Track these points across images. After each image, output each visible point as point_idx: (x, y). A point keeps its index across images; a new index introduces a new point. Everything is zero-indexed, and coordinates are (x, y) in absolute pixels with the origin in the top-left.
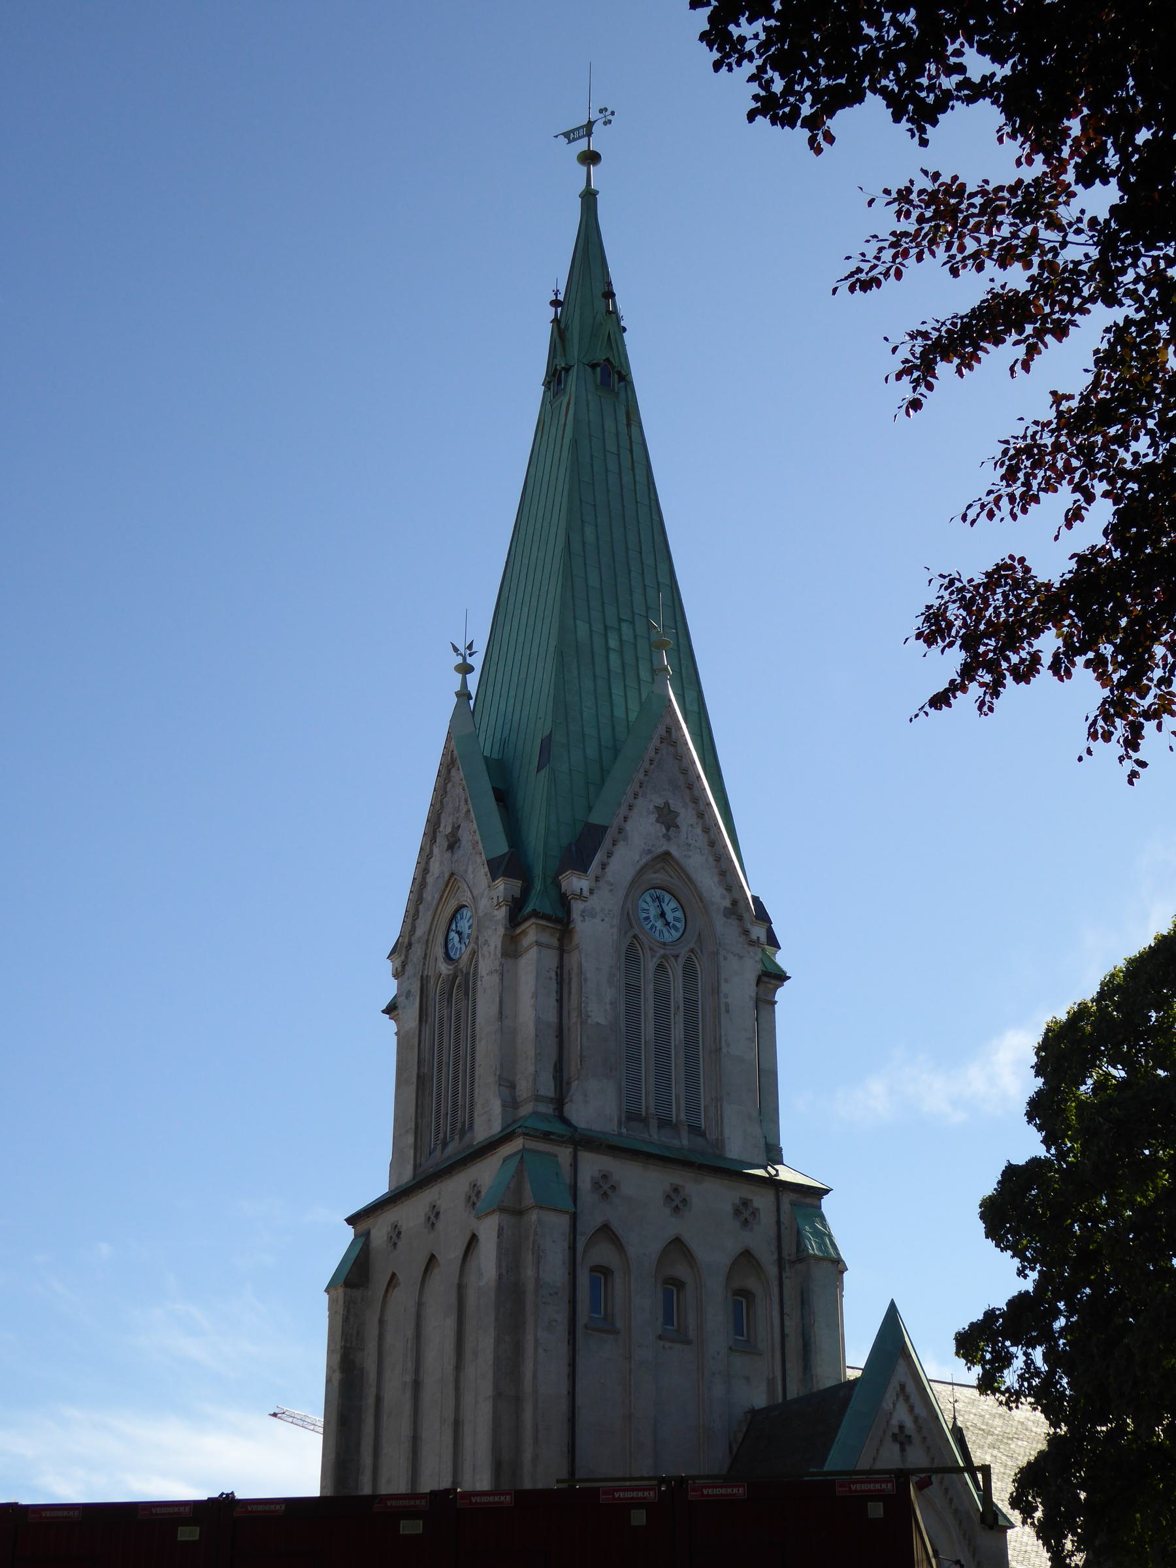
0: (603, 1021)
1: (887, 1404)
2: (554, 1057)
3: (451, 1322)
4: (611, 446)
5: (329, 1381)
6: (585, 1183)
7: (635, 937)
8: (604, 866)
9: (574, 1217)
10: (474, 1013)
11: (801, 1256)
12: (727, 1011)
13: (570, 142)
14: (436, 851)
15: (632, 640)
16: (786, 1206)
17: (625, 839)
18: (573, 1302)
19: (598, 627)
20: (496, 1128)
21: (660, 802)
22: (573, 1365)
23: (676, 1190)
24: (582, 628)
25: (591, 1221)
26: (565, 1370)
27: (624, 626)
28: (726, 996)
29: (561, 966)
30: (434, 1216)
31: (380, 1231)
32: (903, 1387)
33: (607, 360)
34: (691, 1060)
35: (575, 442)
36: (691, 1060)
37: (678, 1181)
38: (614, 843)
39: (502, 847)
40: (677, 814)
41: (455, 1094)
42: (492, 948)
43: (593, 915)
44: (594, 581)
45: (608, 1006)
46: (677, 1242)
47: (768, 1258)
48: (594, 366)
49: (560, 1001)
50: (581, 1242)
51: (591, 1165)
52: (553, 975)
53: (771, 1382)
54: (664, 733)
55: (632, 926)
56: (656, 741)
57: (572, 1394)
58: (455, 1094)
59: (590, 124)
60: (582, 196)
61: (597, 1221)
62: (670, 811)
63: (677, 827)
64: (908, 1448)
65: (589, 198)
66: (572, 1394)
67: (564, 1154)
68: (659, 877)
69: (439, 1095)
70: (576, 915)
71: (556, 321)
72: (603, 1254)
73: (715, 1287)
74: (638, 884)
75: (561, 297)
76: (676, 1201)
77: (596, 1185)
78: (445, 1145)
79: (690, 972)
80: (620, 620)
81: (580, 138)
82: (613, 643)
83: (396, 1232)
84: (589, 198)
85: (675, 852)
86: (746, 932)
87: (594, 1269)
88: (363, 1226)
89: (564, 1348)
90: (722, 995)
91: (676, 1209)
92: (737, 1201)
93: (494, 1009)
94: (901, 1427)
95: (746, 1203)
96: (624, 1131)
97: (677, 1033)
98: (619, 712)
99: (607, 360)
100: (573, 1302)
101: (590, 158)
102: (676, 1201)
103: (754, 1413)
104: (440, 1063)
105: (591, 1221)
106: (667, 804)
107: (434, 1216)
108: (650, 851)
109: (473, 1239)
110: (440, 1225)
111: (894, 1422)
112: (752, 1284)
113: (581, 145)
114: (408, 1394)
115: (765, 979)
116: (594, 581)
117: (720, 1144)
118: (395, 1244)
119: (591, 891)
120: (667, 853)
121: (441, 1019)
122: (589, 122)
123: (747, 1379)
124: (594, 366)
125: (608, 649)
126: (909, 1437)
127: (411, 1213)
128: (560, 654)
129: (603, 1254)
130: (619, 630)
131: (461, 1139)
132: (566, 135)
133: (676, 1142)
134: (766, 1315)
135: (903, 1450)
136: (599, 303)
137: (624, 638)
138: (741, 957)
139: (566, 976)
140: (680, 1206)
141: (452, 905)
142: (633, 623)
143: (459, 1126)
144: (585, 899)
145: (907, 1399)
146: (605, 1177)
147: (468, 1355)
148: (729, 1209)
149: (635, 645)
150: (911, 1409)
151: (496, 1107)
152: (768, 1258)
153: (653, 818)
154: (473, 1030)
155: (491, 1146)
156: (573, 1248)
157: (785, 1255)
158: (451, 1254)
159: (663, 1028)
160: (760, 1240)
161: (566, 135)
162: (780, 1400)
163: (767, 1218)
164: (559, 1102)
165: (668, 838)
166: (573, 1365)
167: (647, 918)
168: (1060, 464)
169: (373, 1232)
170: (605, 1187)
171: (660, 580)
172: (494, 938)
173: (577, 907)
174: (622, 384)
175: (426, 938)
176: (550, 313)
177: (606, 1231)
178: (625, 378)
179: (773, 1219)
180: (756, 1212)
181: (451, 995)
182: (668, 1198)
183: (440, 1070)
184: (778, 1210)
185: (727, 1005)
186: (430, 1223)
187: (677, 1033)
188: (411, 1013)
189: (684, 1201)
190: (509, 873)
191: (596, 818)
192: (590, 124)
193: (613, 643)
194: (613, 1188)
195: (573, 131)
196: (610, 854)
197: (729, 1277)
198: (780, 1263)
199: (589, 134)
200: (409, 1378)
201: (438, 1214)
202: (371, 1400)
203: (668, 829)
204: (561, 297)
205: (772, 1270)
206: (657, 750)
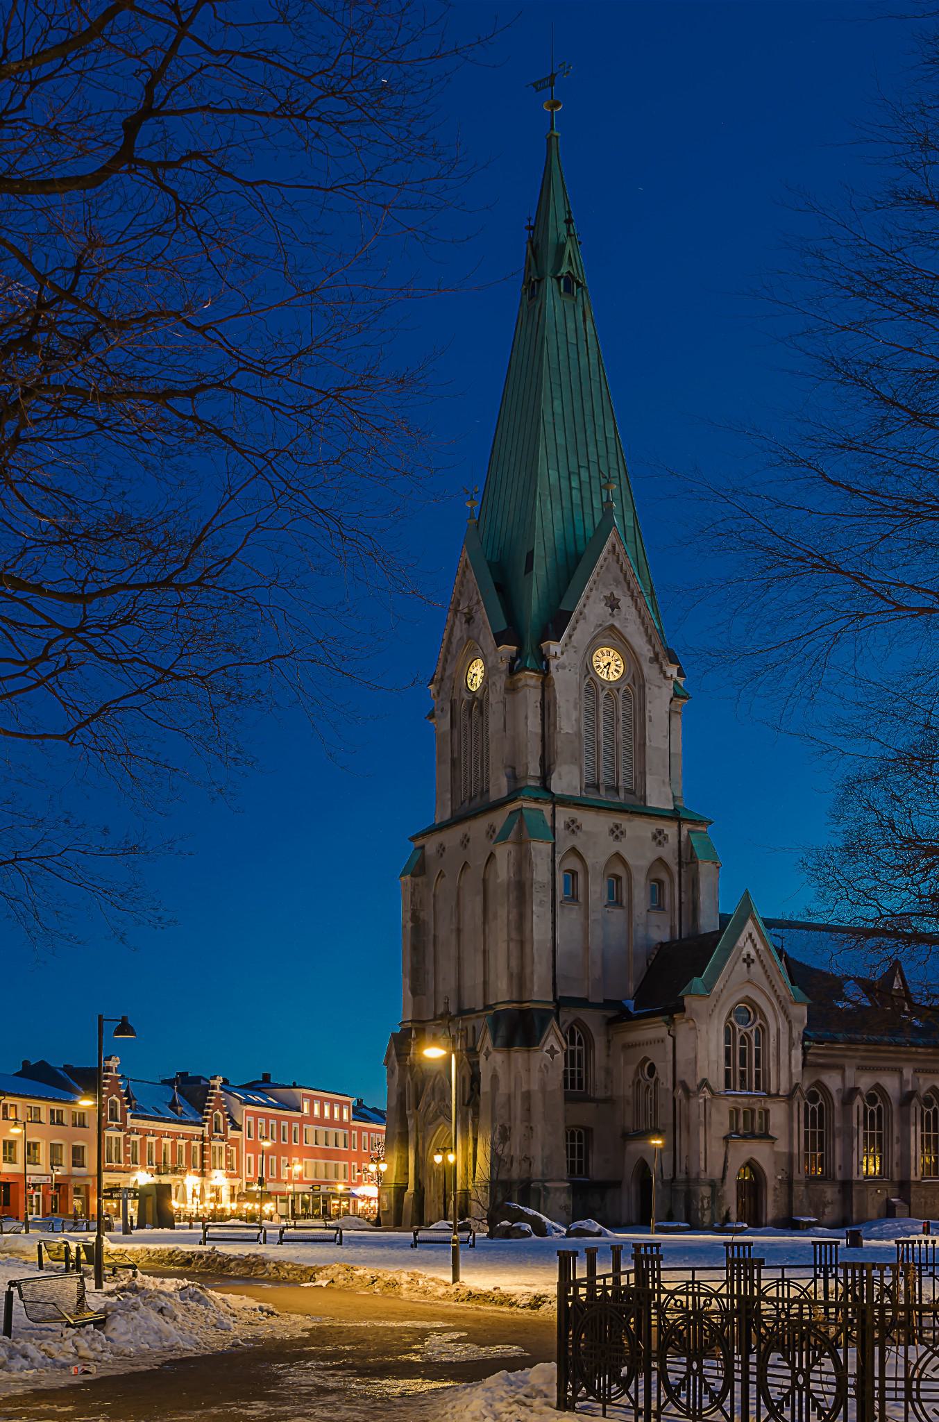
1: (740, 943)
2: (540, 752)
6: (560, 825)
7: (591, 679)
8: (570, 637)
10: (487, 725)
12: (650, 721)
13: (537, 91)
14: (457, 622)
18: (554, 890)
19: (564, 473)
20: (505, 793)
21: (608, 593)
22: (554, 923)
23: (617, 827)
26: (550, 925)
27: (582, 470)
30: (465, 841)
32: (750, 935)
33: (569, 272)
37: (618, 822)
38: (577, 622)
39: (503, 625)
40: (619, 600)
41: (476, 771)
43: (564, 668)
46: (618, 855)
50: (558, 860)
51: (563, 814)
53: (672, 928)
54: (611, 548)
55: (589, 673)
61: (569, 846)
62: (615, 599)
64: (752, 966)
67: (547, 809)
70: (552, 669)
76: (617, 833)
77: (568, 826)
78: (471, 799)
82: (575, 484)
83: (442, 849)
85: (617, 625)
86: (664, 673)
89: (549, 916)
94: (749, 955)
95: (660, 832)
96: (584, 794)
98: (580, 532)
99: (569, 272)
100: (554, 890)
103: (662, 944)
106: (612, 594)
108: (601, 625)
110: (470, 845)
111: (744, 952)
112: (663, 876)
116: (561, 440)
120: (613, 626)
121: (465, 726)
123: (658, 926)
125: (571, 488)
126: (753, 961)
131: (481, 797)
132: (534, 85)
133: (616, 800)
135: (749, 966)
137: (582, 479)
138: (660, 687)
142: (588, 468)
145: (753, 941)
146: (573, 822)
147: (490, 916)
150: (755, 946)
151: (504, 781)
153: (603, 604)
156: (553, 861)
166: (554, 923)
167: (599, 666)
168: (780, 1307)
170: (573, 826)
173: (553, 663)
180: (666, 837)
181: (471, 712)
182: (612, 832)
185: (650, 717)
189: (622, 833)
191: (564, 607)
193: (575, 484)
194: (578, 827)
196: (574, 629)
198: (680, 864)
200: (454, 927)
201: (468, 841)
202: (431, 937)
203: (613, 610)
204: (532, 224)
205: (675, 868)
206: (605, 560)
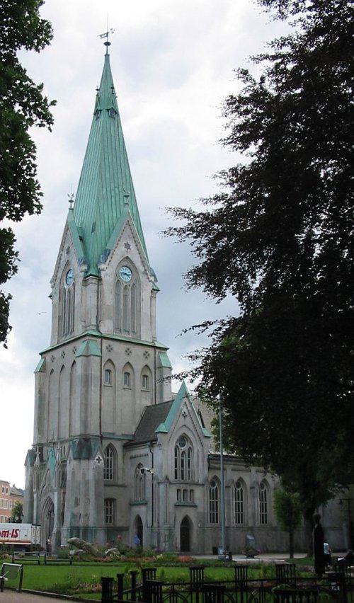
3: (68, 383)
4: (113, 135)
5: (35, 396)
6: (104, 348)
11: (161, 367)
16: (157, 353)
18: (101, 379)
19: (109, 189)
23: (146, 352)
24: (105, 190)
31: (49, 356)
34: (133, 313)
35: (102, 134)
36: (133, 313)
44: (108, 176)
47: (152, 367)
48: (108, 110)
56: (124, 225)
59: (107, 33)
60: (105, 56)
65: (107, 56)
68: (125, 263)
71: (97, 95)
72: (109, 366)
73: (138, 376)
74: (120, 265)
76: (128, 352)
79: (133, 289)
84: (107, 56)
86: (148, 278)
87: (107, 370)
88: (44, 356)
89: (99, 392)
93: (80, 300)
97: (130, 306)
100: (101, 379)
101: (107, 44)
102: (128, 352)
107: (63, 355)
112: (148, 373)
113: (105, 40)
116: (108, 176)
124: (108, 110)
127: (57, 353)
128: (98, 198)
129: (109, 366)
132: (101, 36)
133: (128, 336)
134: (151, 380)
136: (110, 90)
141: (68, 269)
144: (104, 270)
148: (124, 351)
152: (152, 367)
158: (68, 366)
159: (125, 305)
160: (151, 364)
161: (101, 36)
163: (152, 356)
164: (98, 327)
172: (80, 280)
173: (103, 273)
176: (96, 92)
178: (117, 113)
182: (144, 354)
186: (139, 478)
187: (130, 306)
188: (56, 298)
190: (84, 263)
192: (107, 33)
197: (142, 371)
199: (107, 36)
202: (47, 402)
205: (153, 370)
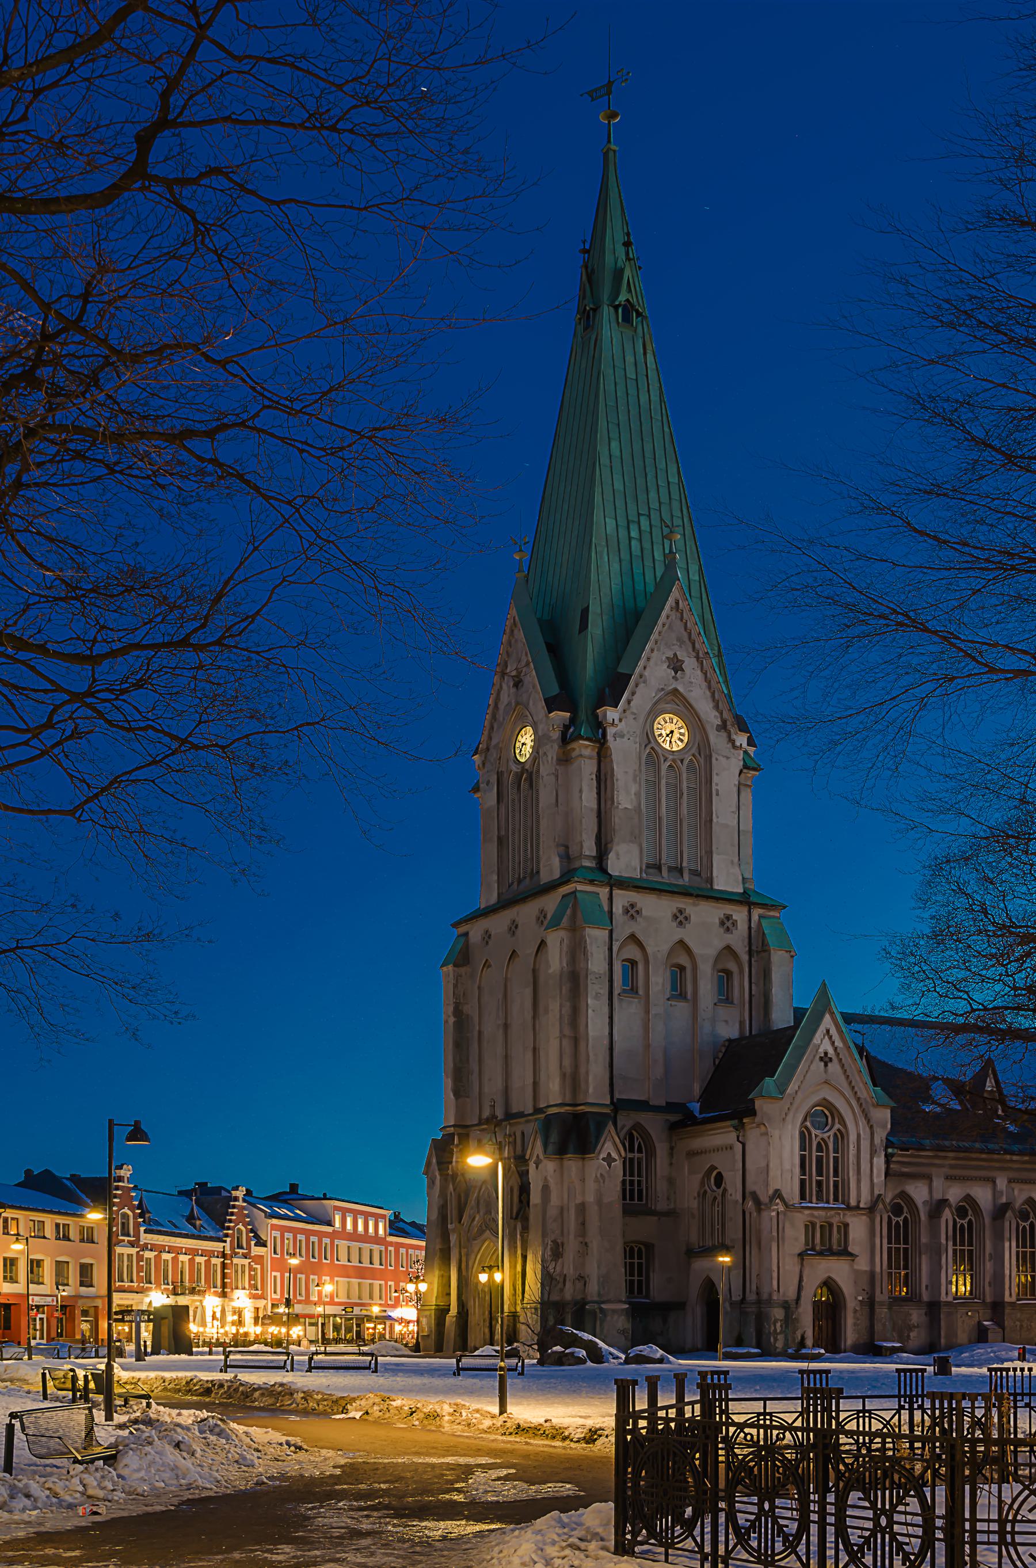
0: (629, 807)
1: (817, 1039)
3: (528, 992)
6: (618, 909)
7: (652, 748)
8: (629, 702)
9: (611, 932)
12: (717, 795)
13: (593, 100)
14: (505, 686)
15: (648, 529)
16: (755, 917)
17: (645, 682)
19: (622, 522)
20: (557, 874)
21: (670, 654)
22: (611, 1018)
23: (681, 911)
25: (622, 933)
26: (607, 1020)
27: (642, 518)
28: (717, 785)
29: (599, 770)
30: (513, 928)
32: (828, 1031)
33: (628, 300)
41: (526, 850)
42: (550, 759)
45: (633, 796)
49: (599, 794)
50: (615, 948)
51: (622, 898)
52: (594, 777)
53: (742, 1023)
55: (650, 742)
57: (611, 1034)
58: (526, 850)
61: (627, 933)
62: (678, 660)
63: (683, 670)
64: (829, 1065)
66: (611, 1034)
67: (604, 892)
69: (514, 850)
70: (609, 737)
72: (632, 952)
75: (587, 246)
76: (681, 918)
77: (626, 911)
78: (520, 881)
80: (639, 515)
81: (601, 96)
83: (487, 935)
85: (681, 689)
89: (606, 1009)
90: (713, 785)
91: (681, 923)
92: (722, 916)
94: (826, 1054)
95: (728, 917)
96: (644, 875)
99: (628, 300)
102: (681, 918)
104: (514, 829)
105: (622, 933)
106: (675, 655)
108: (663, 689)
109: (543, 944)
111: (821, 1050)
112: (732, 966)
114: (501, 1031)
115: (745, 771)
116: (618, 486)
117: (710, 880)
118: (487, 943)
119: (620, 720)
120: (676, 690)
122: (609, 82)
125: (630, 538)
126: (831, 1060)
129: (632, 952)
130: (639, 523)
133: (680, 882)
135: (826, 1065)
137: (643, 528)
138: (728, 758)
139: (602, 777)
140: (678, 915)
142: (649, 516)
143: (529, 871)
145: (830, 1038)
146: (632, 906)
149: (651, 533)
150: (833, 1043)
151: (556, 862)
153: (665, 666)
154: (537, 811)
155: (552, 886)
156: (611, 949)
157: (754, 948)
162: (748, 1034)
165: (675, 678)
167: (661, 735)
169: (471, 934)
170: (632, 912)
171: (670, 480)
173: (611, 731)
174: (640, 319)
175: (167, 13)
177: (633, 938)
179: (746, 927)
180: (734, 924)
182: (675, 917)
183: (513, 834)
184: (750, 920)
185: (717, 791)
194: (638, 912)
195: (596, 90)
196: (633, 694)
198: (750, 953)
201: (516, 927)
202: (476, 1034)
203: (676, 673)
205: (745, 958)
